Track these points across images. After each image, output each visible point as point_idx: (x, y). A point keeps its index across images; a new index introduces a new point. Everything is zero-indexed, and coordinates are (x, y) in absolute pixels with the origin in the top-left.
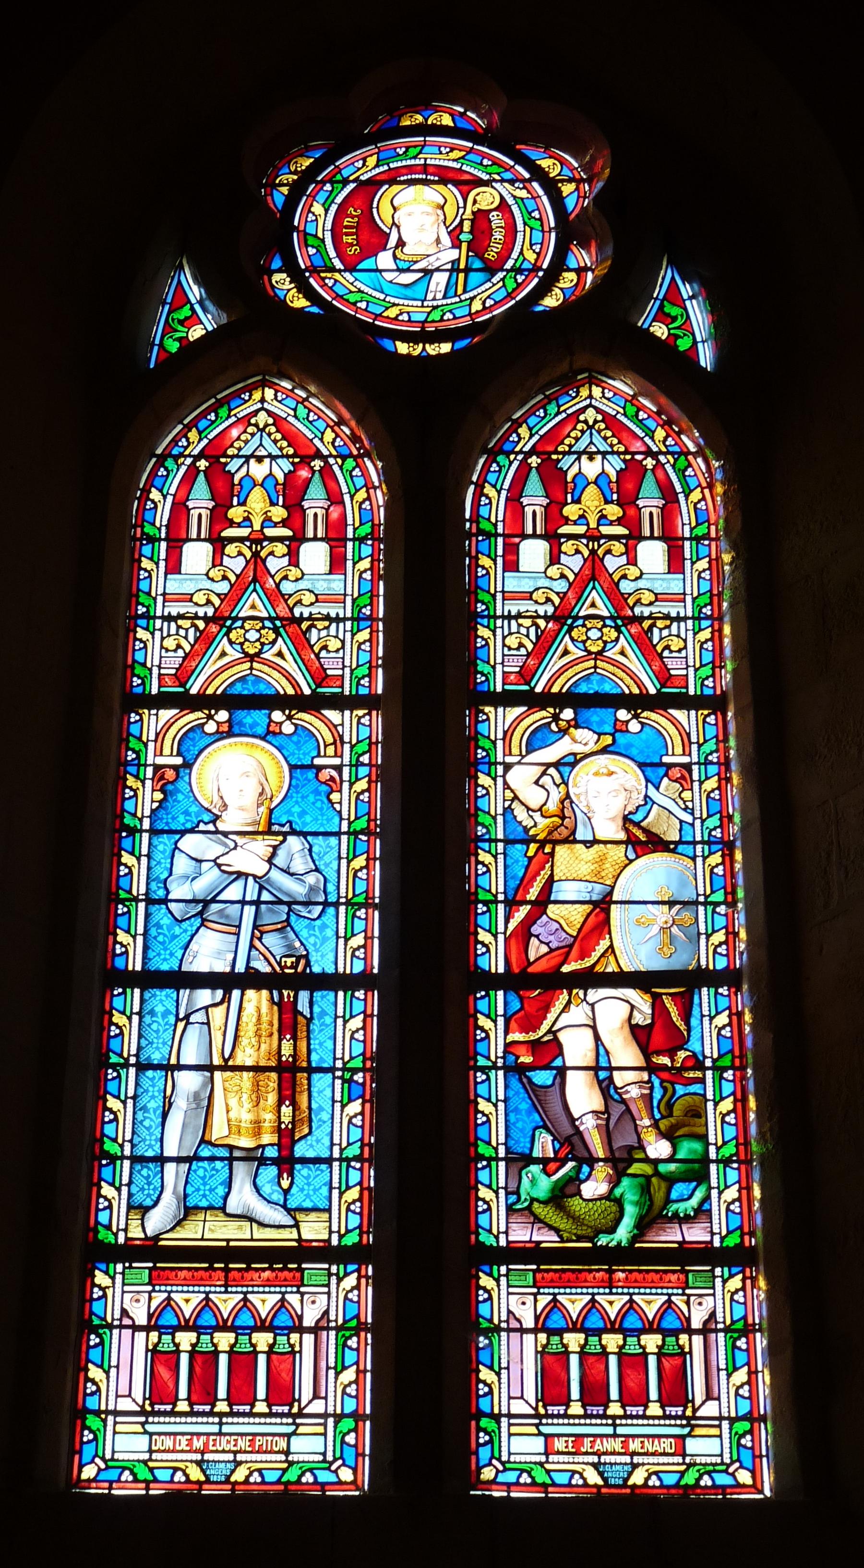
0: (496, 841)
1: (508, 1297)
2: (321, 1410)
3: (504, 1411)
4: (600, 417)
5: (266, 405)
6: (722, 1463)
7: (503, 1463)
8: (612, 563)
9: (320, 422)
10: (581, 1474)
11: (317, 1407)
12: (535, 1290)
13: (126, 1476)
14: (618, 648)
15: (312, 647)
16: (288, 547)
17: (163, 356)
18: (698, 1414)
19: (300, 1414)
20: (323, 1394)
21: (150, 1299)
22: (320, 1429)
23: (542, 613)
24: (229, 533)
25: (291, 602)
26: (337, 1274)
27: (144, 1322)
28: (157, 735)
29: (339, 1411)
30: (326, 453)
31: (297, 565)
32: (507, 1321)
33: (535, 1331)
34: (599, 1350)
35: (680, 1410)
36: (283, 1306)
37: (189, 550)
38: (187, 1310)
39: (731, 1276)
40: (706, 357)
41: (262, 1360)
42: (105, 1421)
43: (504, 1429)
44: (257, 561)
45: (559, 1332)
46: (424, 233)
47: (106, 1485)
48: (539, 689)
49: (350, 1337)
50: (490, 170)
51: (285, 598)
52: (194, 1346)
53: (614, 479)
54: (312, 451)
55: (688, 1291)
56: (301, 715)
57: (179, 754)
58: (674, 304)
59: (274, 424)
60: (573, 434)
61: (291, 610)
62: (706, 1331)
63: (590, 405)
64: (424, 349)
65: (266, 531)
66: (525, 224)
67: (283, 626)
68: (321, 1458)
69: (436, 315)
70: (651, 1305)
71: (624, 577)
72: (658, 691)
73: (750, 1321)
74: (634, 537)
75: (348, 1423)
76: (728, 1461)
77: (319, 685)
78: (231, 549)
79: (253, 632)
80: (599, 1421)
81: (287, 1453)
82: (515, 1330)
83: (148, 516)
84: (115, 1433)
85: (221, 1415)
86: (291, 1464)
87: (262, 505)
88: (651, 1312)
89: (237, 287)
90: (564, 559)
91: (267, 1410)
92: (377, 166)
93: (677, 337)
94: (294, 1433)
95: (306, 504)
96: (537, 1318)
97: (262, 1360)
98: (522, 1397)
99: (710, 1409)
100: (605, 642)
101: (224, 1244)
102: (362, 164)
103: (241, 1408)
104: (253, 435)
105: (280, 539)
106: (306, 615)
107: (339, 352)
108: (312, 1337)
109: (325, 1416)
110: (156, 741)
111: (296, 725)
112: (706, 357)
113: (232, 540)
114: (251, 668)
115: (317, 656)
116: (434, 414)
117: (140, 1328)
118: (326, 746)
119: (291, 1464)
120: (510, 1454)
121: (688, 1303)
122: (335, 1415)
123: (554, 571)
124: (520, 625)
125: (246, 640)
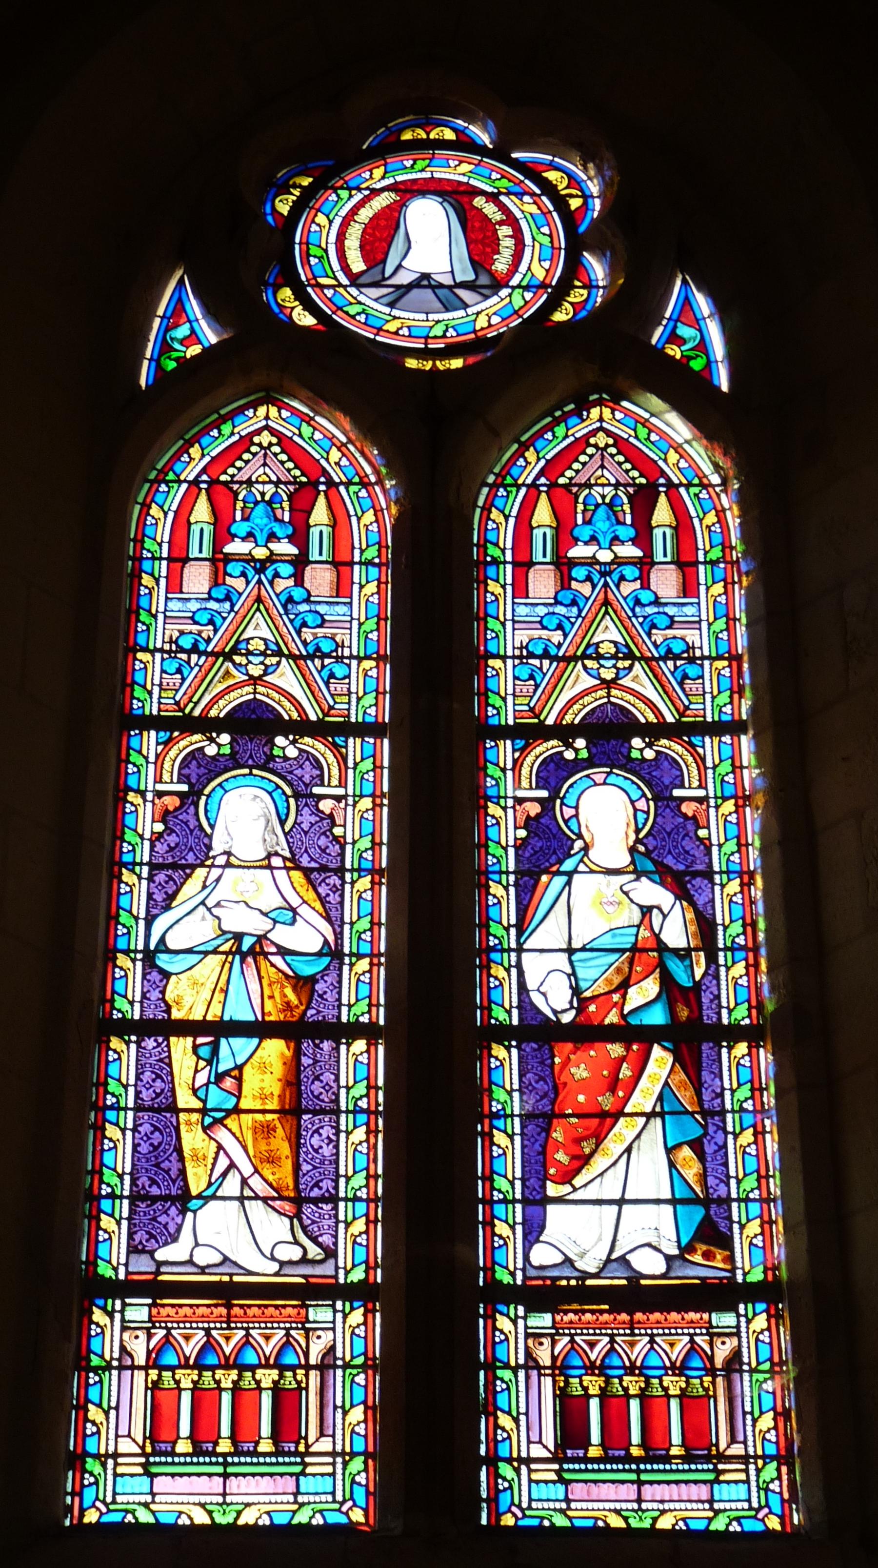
0: (507, 873)
2: (329, 1448)
4: (611, 441)
5: (605, 425)
6: (334, 1501)
9: (328, 438)
11: (325, 1445)
18: (312, 1450)
19: (307, 1453)
20: (741, 1438)
22: (329, 1469)
33: (146, 1368)
39: (352, 1309)
40: (723, 382)
45: (252, 1368)
46: (425, 246)
49: (765, 1380)
50: (497, 184)
56: (307, 740)
62: (327, 1365)
64: (434, 364)
68: (746, 1505)
73: (370, 1355)
80: (248, 1460)
81: (711, 1501)
83: (149, 531)
86: (717, 1512)
92: (383, 178)
93: (690, 358)
94: (303, 1473)
96: (149, 1353)
99: (325, 1445)
101: (541, 1282)
104: (591, 456)
108: (143, 1373)
109: (333, 1454)
111: (300, 750)
112: (723, 382)
114: (255, 693)
119: (717, 1512)
121: (307, 1338)
122: (343, 1454)
123: (219, 593)
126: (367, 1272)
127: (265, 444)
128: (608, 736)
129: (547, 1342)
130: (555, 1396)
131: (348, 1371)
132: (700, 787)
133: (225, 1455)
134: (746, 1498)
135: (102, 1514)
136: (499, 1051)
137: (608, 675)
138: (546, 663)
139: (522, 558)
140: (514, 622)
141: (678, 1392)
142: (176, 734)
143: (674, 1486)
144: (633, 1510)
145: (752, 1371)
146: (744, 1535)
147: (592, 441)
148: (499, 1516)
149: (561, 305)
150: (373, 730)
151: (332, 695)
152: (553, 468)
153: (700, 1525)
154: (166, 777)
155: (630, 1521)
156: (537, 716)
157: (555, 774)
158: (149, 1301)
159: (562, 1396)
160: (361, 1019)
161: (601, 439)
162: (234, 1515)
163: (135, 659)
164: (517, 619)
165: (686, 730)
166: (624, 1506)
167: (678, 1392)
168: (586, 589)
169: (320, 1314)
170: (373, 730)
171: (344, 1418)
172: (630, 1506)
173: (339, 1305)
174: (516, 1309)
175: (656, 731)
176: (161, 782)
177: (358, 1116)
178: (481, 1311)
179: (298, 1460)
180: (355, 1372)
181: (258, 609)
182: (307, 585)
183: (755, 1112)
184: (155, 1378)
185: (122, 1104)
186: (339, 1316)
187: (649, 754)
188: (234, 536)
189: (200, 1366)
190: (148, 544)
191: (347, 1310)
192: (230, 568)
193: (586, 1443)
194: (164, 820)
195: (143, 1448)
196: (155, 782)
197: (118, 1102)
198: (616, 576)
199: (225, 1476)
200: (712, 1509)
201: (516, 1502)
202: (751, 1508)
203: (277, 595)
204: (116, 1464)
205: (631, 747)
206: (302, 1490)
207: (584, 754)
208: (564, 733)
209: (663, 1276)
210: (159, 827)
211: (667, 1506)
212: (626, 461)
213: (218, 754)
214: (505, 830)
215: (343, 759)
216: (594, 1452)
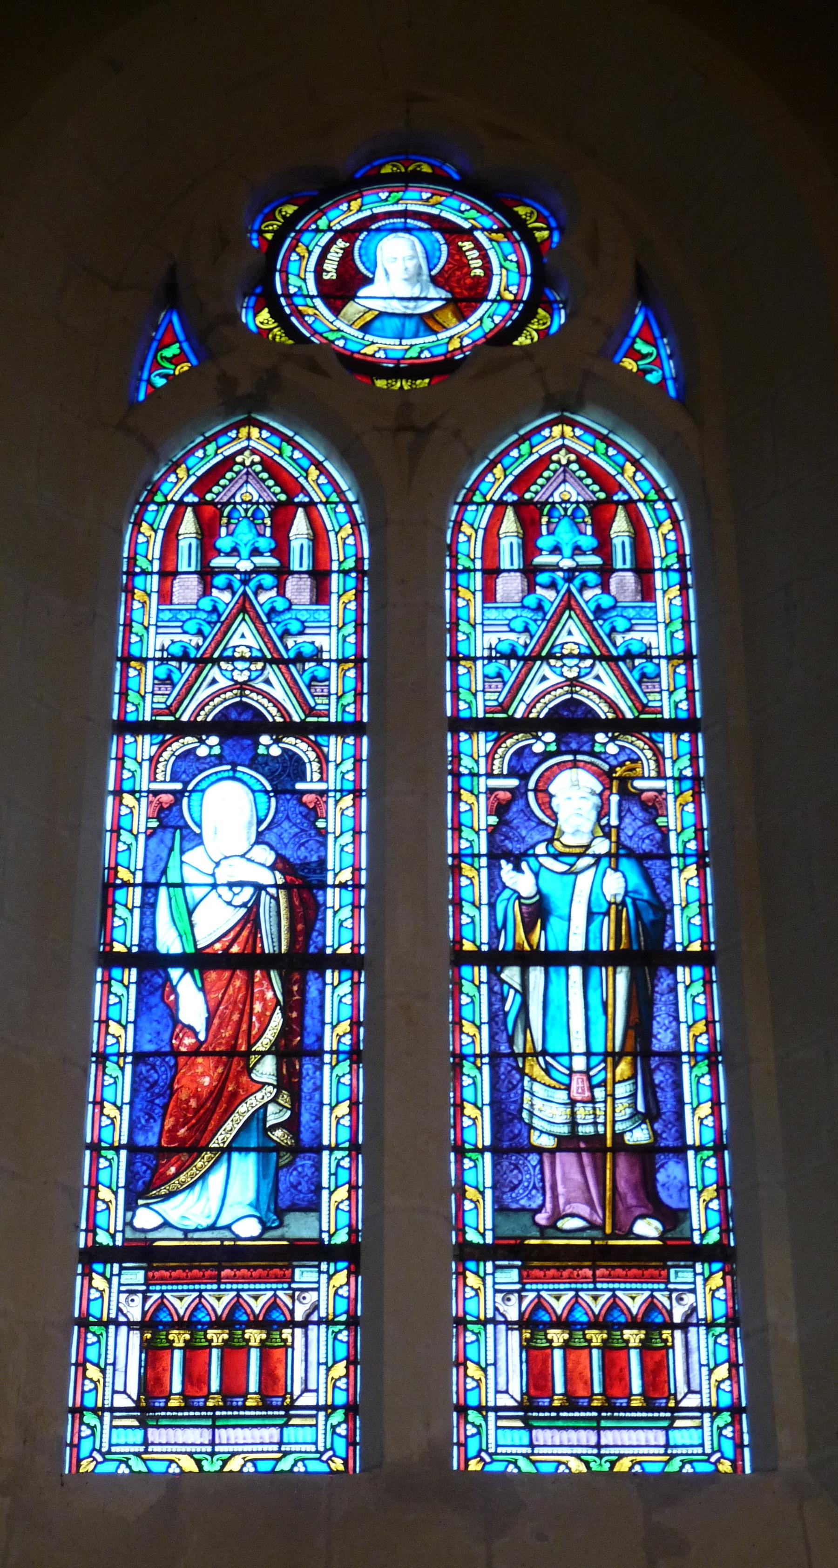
0: (479, 856)
1: (490, 1292)
2: (313, 1402)
3: (108, 1404)
4: (573, 457)
5: (567, 442)
6: (703, 1454)
7: (490, 1455)
17: (151, 390)
18: (297, 1403)
19: (292, 1406)
26: (327, 1272)
27: (138, 1318)
36: (577, 1302)
38: (559, 1306)
42: (486, 1418)
46: (393, 277)
58: (647, 342)
66: (502, 266)
70: (634, 1301)
75: (726, 1417)
76: (321, 1449)
78: (220, 580)
84: (112, 1427)
87: (571, 535)
88: (559, 1306)
90: (539, 590)
94: (286, 1425)
101: (218, 1243)
109: (317, 1408)
118: (168, 761)
120: (497, 1446)
121: (670, 1298)
127: (248, 463)
129: (514, 1298)
130: (522, 1347)
131: (331, 1329)
132: (321, 780)
133: (214, 1409)
134: (699, 1443)
135: (486, 1463)
137: (242, 678)
138: (184, 665)
139: (490, 565)
140: (157, 627)
141: (182, 1344)
142: (168, 737)
143: (556, 1431)
144: (206, 1453)
146: (696, 1476)
148: (467, 1460)
150: (354, 729)
151: (645, 693)
152: (203, 484)
153: (656, 1468)
154: (160, 777)
155: (592, 1465)
156: (173, 714)
157: (188, 767)
159: (527, 1347)
161: (562, 456)
162: (220, 1463)
164: (487, 625)
165: (313, 729)
166: (584, 1451)
167: (182, 1344)
168: (226, 596)
169: (304, 1275)
170: (354, 729)
172: (590, 1451)
173: (324, 1266)
175: (284, 729)
176: (155, 780)
179: (282, 1413)
182: (288, 594)
186: (324, 1277)
187: (275, 751)
188: (219, 552)
191: (332, 1271)
193: (245, 1395)
194: (158, 818)
196: (150, 782)
198: (577, 582)
199: (213, 1427)
201: (484, 1447)
202: (317, 1452)
203: (261, 605)
205: (595, 741)
206: (285, 1440)
207: (553, 748)
209: (259, 1238)
210: (493, 820)
211: (623, 1451)
212: (270, 478)
213: (545, 751)
215: (659, 756)
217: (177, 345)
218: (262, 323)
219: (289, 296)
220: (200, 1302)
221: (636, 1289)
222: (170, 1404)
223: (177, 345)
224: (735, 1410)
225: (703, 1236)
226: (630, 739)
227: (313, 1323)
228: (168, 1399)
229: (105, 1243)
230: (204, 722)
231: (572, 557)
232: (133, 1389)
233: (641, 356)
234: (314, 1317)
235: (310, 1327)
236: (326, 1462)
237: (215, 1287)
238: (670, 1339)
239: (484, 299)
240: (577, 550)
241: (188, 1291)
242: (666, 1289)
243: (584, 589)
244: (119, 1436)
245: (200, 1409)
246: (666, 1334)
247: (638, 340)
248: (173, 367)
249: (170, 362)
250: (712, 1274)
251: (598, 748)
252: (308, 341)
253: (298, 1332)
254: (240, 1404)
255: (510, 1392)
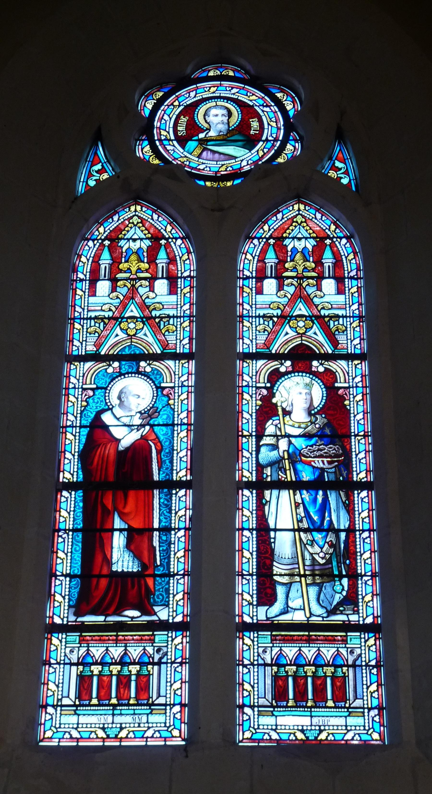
5: (301, 212)
8: (141, 291)
10: (268, 734)
12: (271, 645)
13: (67, 736)
14: (143, 332)
15: (161, 330)
16: (149, 282)
18: (352, 706)
21: (79, 650)
23: (107, 316)
24: (119, 276)
25: (319, 308)
27: (269, 662)
28: (257, 372)
29: (370, 706)
30: (167, 236)
31: (153, 291)
32: (257, 660)
34: (109, 673)
35: (343, 704)
37: (100, 284)
41: (95, 679)
43: (59, 712)
44: (133, 290)
45: (303, 666)
47: (57, 740)
48: (273, 352)
51: (148, 307)
52: (100, 672)
53: (311, 250)
54: (326, 236)
55: (347, 646)
56: (155, 363)
57: (94, 383)
59: (137, 224)
60: (291, 228)
61: (319, 312)
63: (299, 214)
65: (304, 273)
66: (269, 124)
67: (147, 320)
69: (223, 169)
71: (148, 297)
72: (162, 352)
74: (152, 279)
77: (164, 349)
79: (132, 324)
82: (67, 664)
84: (61, 714)
85: (114, 706)
89: (122, 156)
90: (285, 288)
91: (333, 705)
92: (195, 97)
95: (158, 261)
97: (95, 679)
98: (265, 698)
100: (137, 330)
102: (187, 96)
103: (104, 702)
105: (145, 279)
106: (326, 315)
107: (164, 186)
109: (165, 705)
110: (256, 375)
111: (152, 368)
113: (288, 278)
115: (164, 335)
116: (219, 217)
117: (74, 664)
121: (347, 651)
124: (95, 322)
125: (129, 328)
126: (183, 617)
128: (301, 358)
136: (246, 492)
145: (356, 436)
147: (295, 220)
149: (281, 155)
157: (275, 377)
158: (79, 634)
160: (182, 479)
163: (61, 496)
171: (172, 684)
174: (254, 633)
177: (183, 426)
178: (238, 635)
180: (371, 668)
181: (132, 303)
183: (363, 387)
184: (82, 670)
185: (74, 425)
187: (321, 369)
189: (102, 663)
190: (78, 309)
192: (119, 284)
195: (75, 702)
197: (73, 424)
200: (346, 729)
204: (61, 710)
207: (290, 369)
208: (279, 357)
214: (250, 405)
216: (291, 703)
217: (101, 164)
218: (146, 152)
219: (160, 140)
220: (281, 653)
221: (330, 647)
222: (289, 705)
223: (101, 164)
224: (380, 708)
225: (173, 618)
226: (330, 363)
227: (164, 663)
228: (129, 700)
229: (248, 622)
230: (283, 353)
231: (136, 274)
232: (72, 695)
233: (338, 169)
234: (164, 660)
235: (162, 665)
236: (370, 735)
237: (308, 645)
238: (151, 671)
239: (260, 140)
240: (139, 270)
241: (332, 647)
242: (345, 647)
243: (310, 288)
244: (65, 719)
245: (303, 707)
246: (150, 667)
247: (336, 161)
248: (99, 175)
249: (94, 173)
250: (369, 638)
251: (314, 369)
252: (171, 162)
253: (156, 668)
254: (285, 705)
255: (70, 697)
